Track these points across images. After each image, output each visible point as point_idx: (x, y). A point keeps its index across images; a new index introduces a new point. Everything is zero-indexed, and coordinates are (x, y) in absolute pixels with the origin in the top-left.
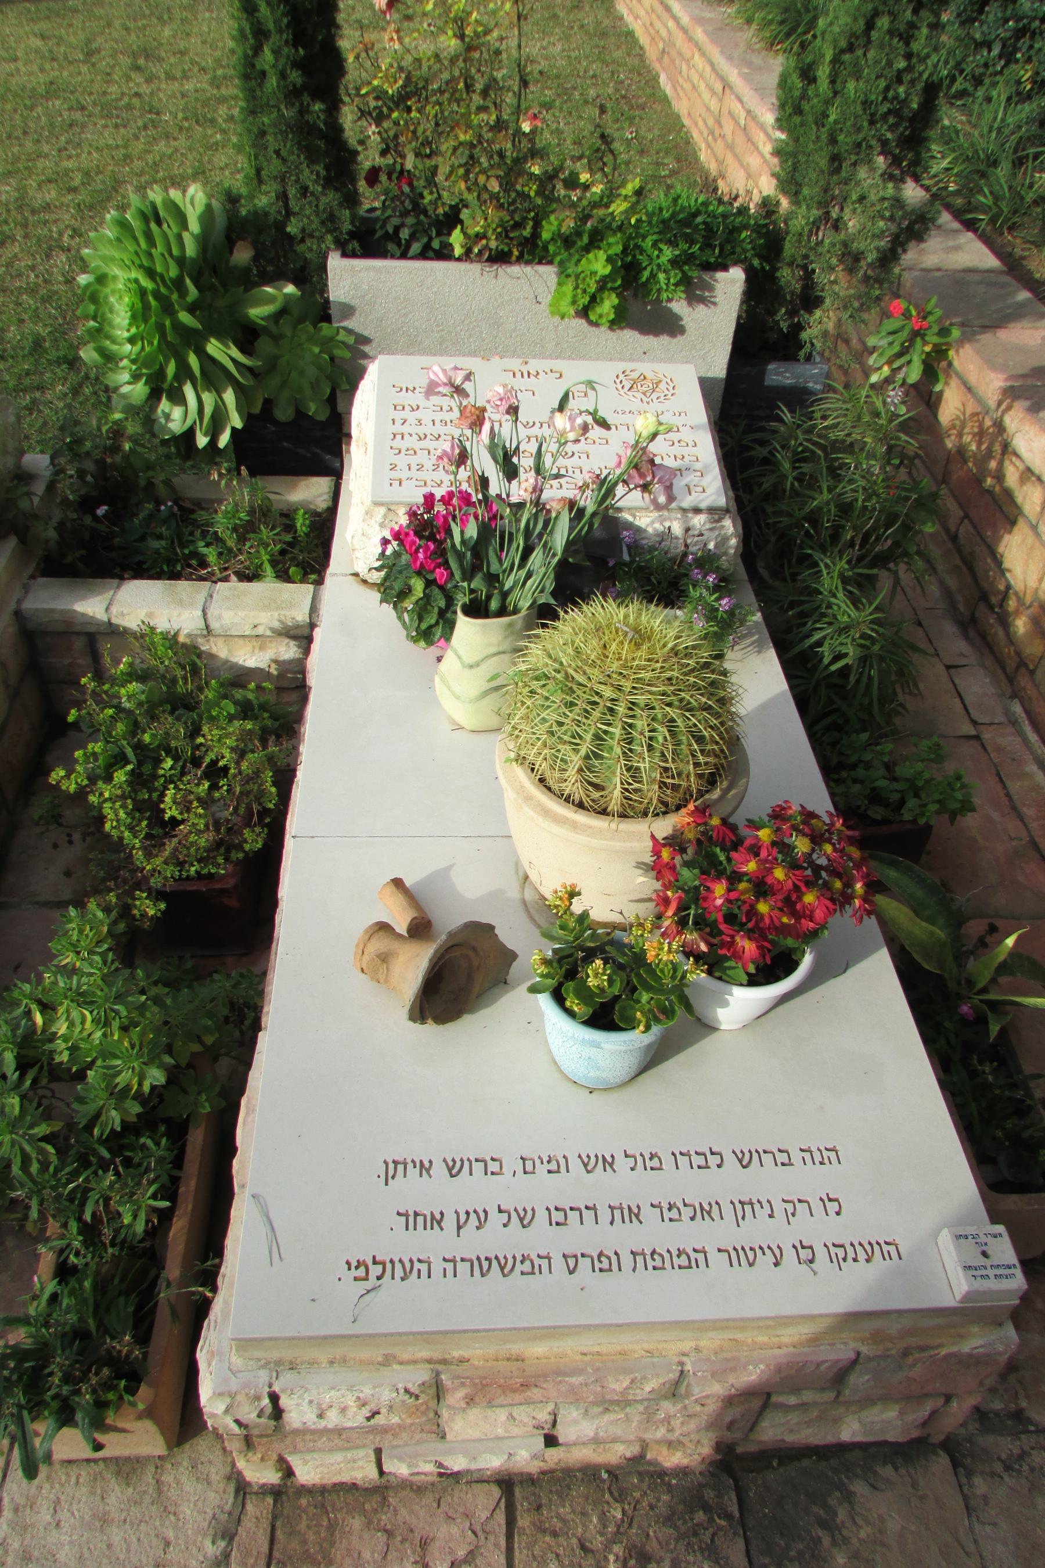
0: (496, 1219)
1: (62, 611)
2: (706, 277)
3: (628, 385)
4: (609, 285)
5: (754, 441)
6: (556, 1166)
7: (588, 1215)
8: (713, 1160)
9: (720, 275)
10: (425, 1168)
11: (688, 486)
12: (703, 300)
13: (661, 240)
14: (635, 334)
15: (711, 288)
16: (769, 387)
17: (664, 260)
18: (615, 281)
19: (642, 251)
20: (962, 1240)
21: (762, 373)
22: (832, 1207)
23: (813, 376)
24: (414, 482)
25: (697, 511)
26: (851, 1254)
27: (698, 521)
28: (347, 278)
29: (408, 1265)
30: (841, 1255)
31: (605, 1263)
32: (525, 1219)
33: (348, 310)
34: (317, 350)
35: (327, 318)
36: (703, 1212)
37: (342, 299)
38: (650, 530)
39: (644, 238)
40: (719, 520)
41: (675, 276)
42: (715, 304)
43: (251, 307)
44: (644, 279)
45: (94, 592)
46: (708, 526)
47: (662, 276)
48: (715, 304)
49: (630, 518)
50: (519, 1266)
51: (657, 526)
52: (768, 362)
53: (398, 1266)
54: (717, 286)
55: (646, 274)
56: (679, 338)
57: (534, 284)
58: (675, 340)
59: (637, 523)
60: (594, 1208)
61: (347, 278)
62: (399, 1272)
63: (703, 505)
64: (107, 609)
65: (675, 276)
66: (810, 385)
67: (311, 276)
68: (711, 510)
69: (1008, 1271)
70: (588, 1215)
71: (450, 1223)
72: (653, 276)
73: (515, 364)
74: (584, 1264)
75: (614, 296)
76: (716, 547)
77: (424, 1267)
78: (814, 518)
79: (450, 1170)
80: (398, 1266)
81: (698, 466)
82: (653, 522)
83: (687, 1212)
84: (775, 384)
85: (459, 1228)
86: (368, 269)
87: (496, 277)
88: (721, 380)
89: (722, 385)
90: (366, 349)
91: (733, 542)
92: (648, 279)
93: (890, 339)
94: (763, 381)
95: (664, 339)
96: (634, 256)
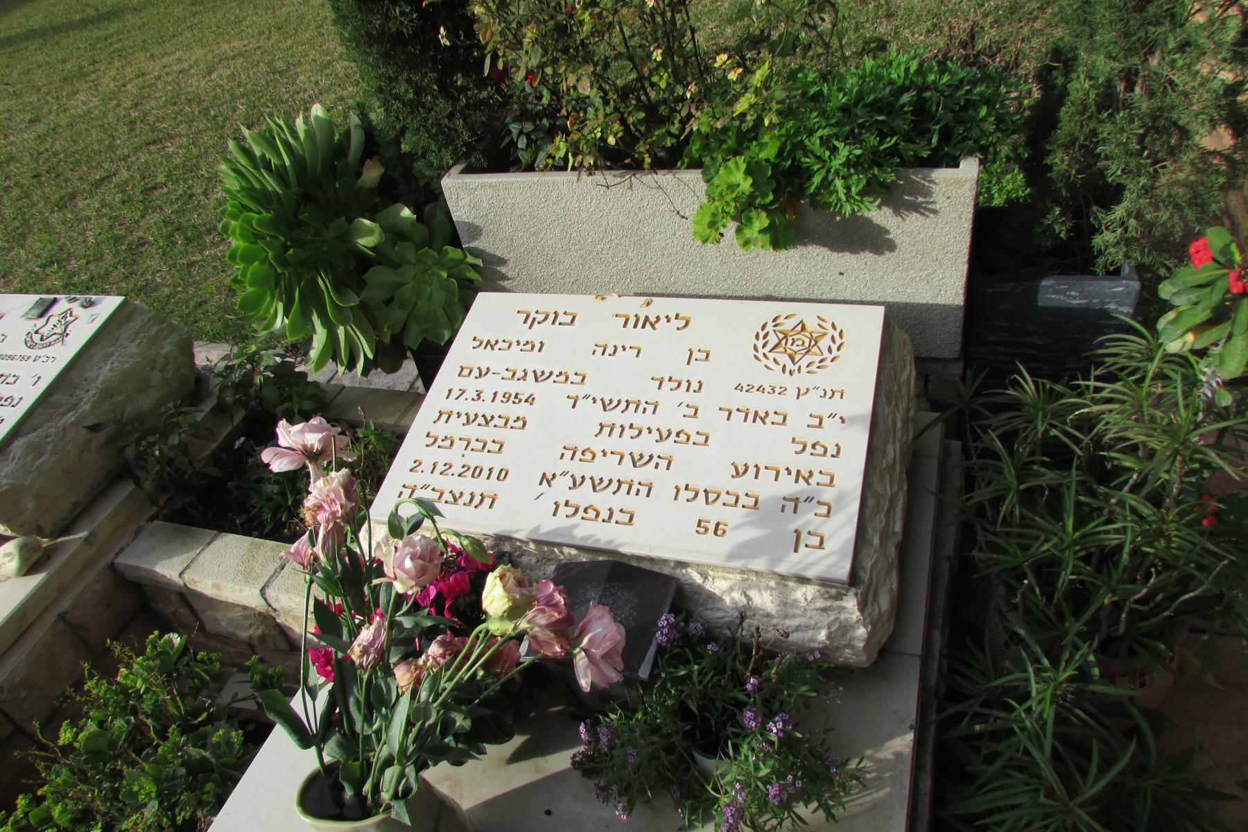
1: (145, 570)
2: (916, 176)
3: (773, 340)
4: (758, 201)
5: (985, 405)
9: (941, 175)
11: (798, 533)
12: (915, 208)
13: (837, 136)
14: (825, 251)
15: (927, 193)
17: (836, 163)
18: (765, 195)
19: (808, 152)
21: (1033, 292)
23: (1114, 296)
25: (803, 580)
27: (804, 594)
28: (467, 194)
33: (475, 231)
34: (445, 275)
35: (455, 241)
37: (464, 219)
38: (727, 599)
39: (811, 133)
40: (839, 597)
41: (858, 182)
42: (935, 212)
43: (362, 237)
44: (812, 189)
45: (171, 554)
46: (820, 604)
47: (839, 183)
48: (935, 212)
49: (698, 579)
51: (737, 595)
52: (1043, 276)
54: (935, 188)
55: (817, 180)
56: (888, 254)
57: (673, 200)
58: (882, 258)
59: (708, 586)
61: (467, 194)
63: (809, 574)
64: (181, 575)
65: (858, 182)
66: (1112, 306)
67: (429, 199)
68: (824, 582)
72: (826, 184)
73: (634, 306)
75: (764, 215)
76: (829, 637)
78: (1047, 570)
81: (828, 495)
82: (731, 589)
84: (1054, 304)
86: (483, 186)
87: (631, 187)
88: (957, 308)
89: (961, 314)
90: (503, 270)
91: (861, 632)
92: (818, 189)
93: (1193, 297)
94: (1036, 299)
95: (867, 257)
96: (794, 159)
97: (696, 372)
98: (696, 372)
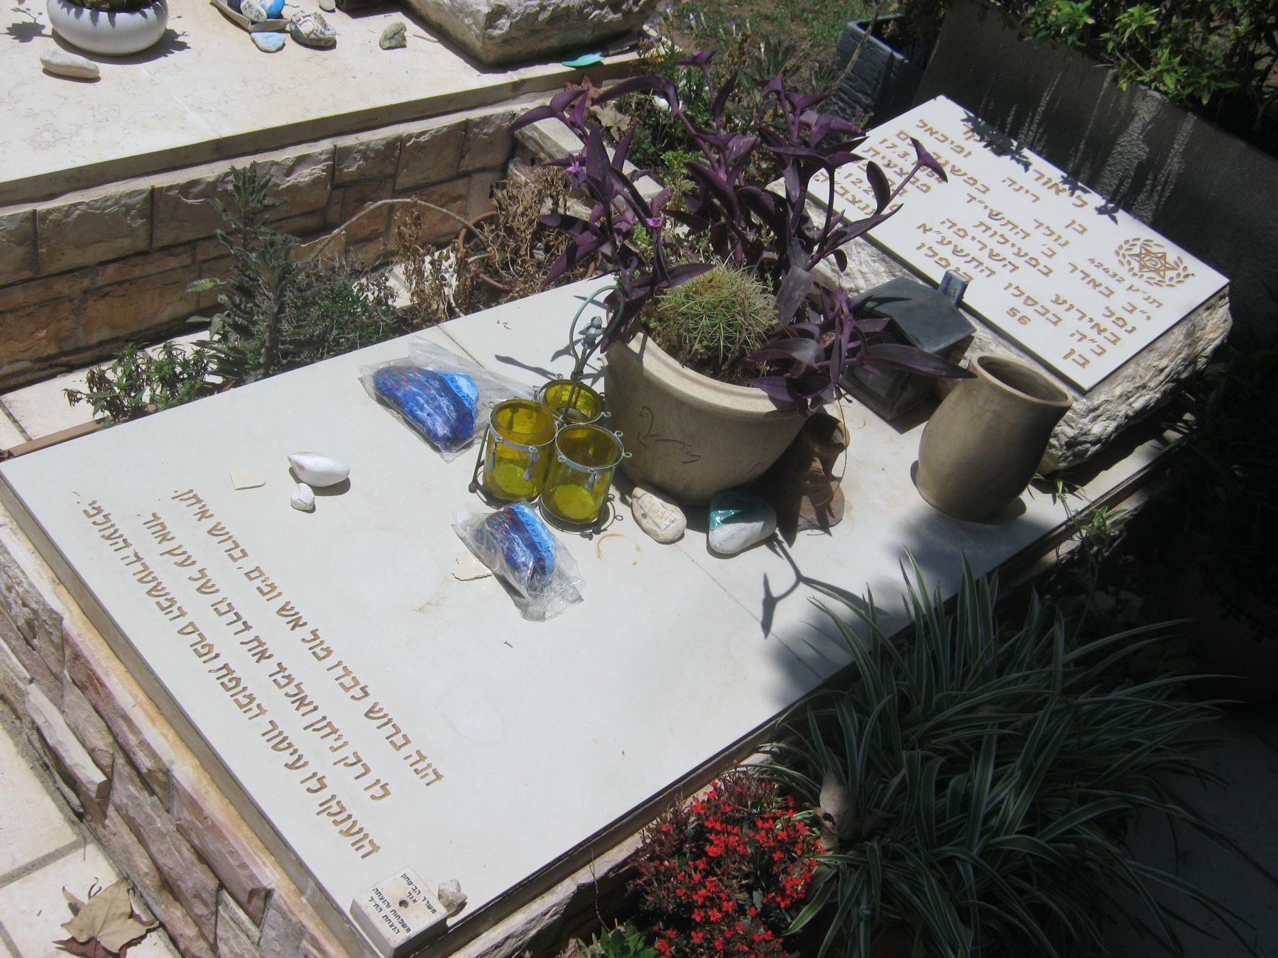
0: (193, 571)
6: (269, 591)
7: (240, 626)
8: (357, 692)
10: (203, 514)
16: (1185, 219)
20: (405, 881)
22: (377, 791)
24: (1093, 346)
26: (339, 818)
29: (355, 829)
30: (333, 810)
31: (205, 650)
32: (205, 588)
36: (205, 588)
50: (161, 600)
53: (350, 822)
60: (367, 770)
62: (107, 533)
69: (399, 926)
70: (240, 626)
71: (168, 546)
74: (195, 638)
77: (256, 711)
79: (370, 711)
80: (350, 822)
83: (291, 689)
85: (169, 552)
97: (1068, 234)
98: (1068, 234)
